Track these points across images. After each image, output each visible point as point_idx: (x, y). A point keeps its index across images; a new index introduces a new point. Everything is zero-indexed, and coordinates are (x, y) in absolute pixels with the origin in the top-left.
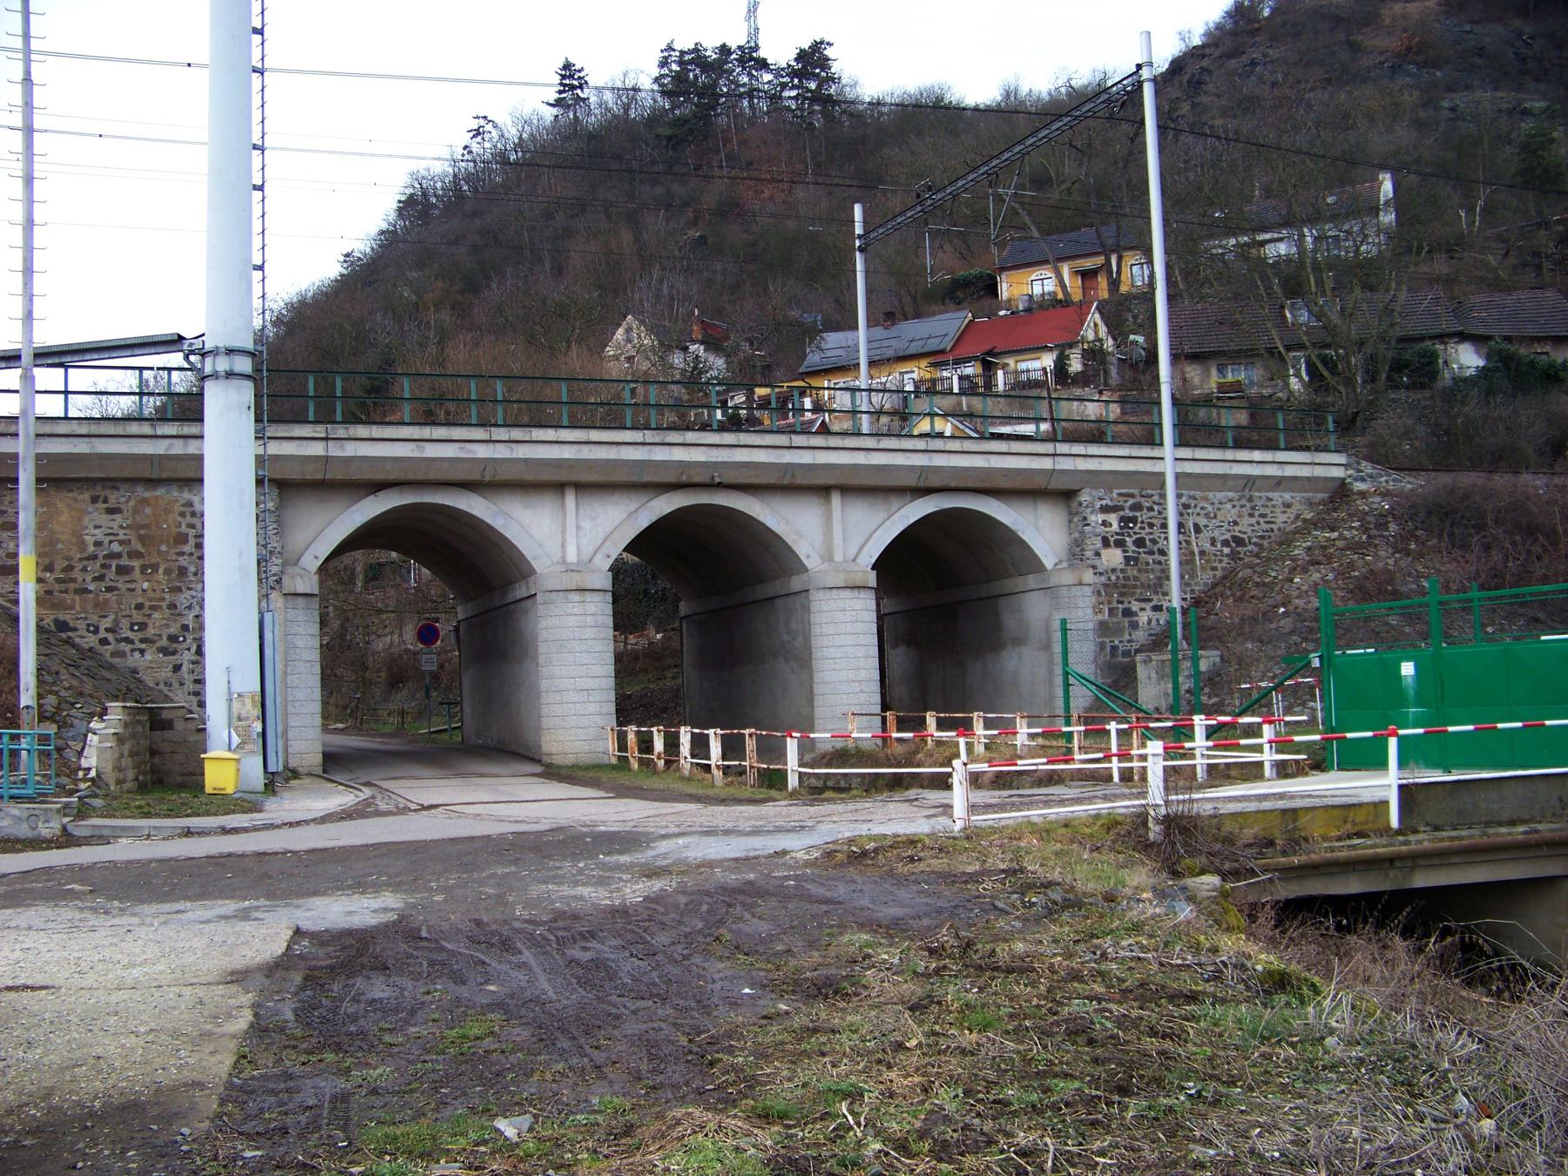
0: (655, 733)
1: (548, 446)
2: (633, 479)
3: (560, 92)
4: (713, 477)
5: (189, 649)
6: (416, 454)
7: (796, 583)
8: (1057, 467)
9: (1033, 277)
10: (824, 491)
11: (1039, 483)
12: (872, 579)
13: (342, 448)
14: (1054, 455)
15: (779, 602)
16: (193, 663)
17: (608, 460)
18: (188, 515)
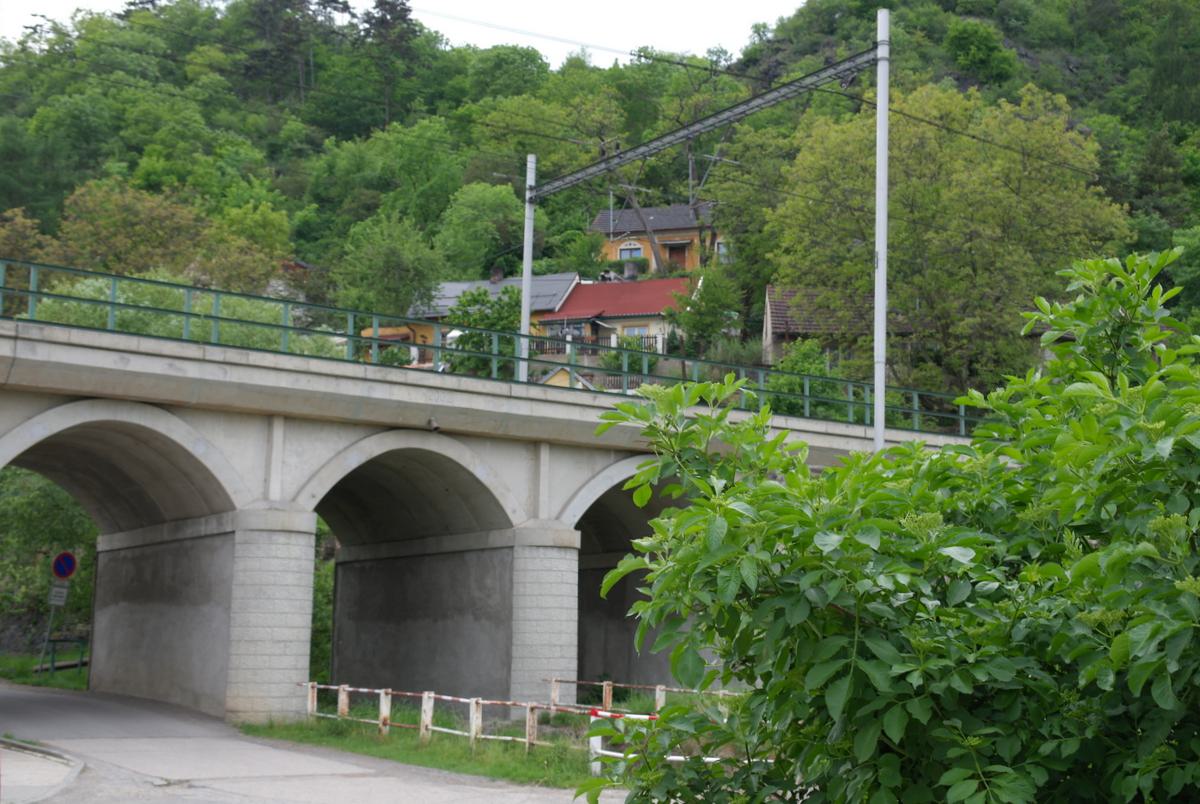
0: (473, 708)
2: (348, 415)
4: (430, 422)
6: (120, 366)
7: (496, 538)
9: (623, 246)
10: (534, 444)
12: (576, 539)
15: (471, 558)
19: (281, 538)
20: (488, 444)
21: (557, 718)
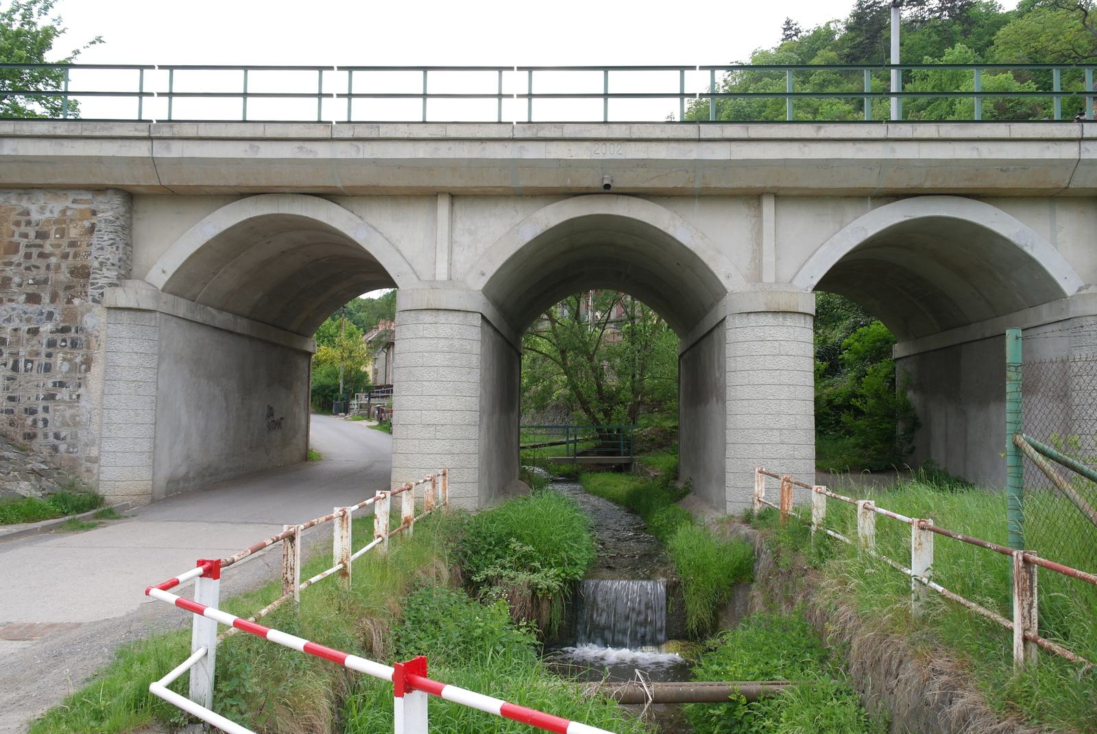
1: (400, 145)
3: (783, 40)
5: (5, 365)
8: (1085, 156)
10: (752, 197)
11: (1056, 180)
13: (168, 149)
14: (1081, 140)
16: (9, 379)
17: (470, 160)
18: (23, 224)
19: (427, 317)
20: (697, 203)
21: (761, 517)
